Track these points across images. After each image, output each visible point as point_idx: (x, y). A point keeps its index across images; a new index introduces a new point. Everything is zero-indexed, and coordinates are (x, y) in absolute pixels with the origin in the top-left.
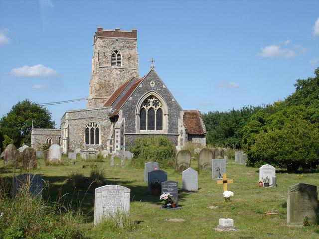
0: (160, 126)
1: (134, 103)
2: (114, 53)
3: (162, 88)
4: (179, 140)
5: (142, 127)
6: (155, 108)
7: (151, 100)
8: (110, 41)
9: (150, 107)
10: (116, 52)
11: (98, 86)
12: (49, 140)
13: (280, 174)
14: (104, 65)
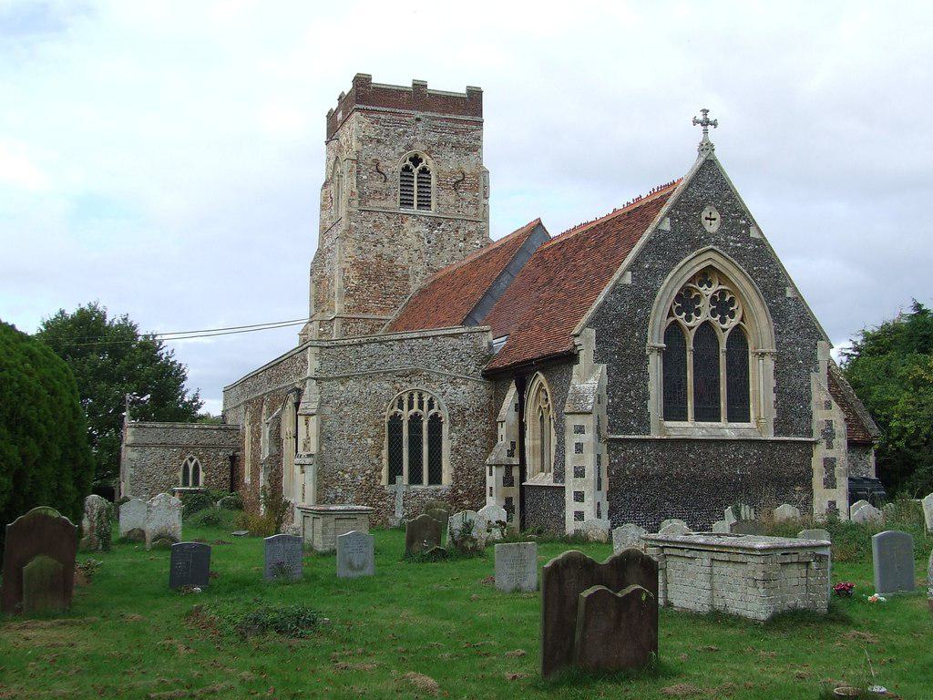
0: (739, 411)
1: (641, 296)
4: (817, 463)
5: (674, 410)
6: (718, 325)
7: (707, 292)
8: (400, 124)
9: (701, 319)
12: (191, 466)
14: (372, 204)
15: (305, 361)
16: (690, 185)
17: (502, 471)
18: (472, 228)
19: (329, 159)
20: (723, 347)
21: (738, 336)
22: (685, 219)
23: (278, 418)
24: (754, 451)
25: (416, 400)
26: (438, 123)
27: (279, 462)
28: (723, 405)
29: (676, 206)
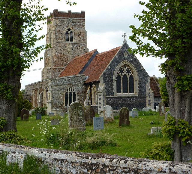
0: (132, 91)
1: (112, 70)
2: (67, 30)
3: (133, 58)
4: (147, 101)
6: (128, 75)
7: (125, 69)
10: (69, 30)
11: (55, 58)
13: (18, 130)
15: (48, 82)
16: (122, 49)
17: (87, 103)
18: (83, 46)
19: (47, 28)
20: (128, 79)
21: (132, 77)
22: (121, 55)
23: (42, 94)
24: (134, 99)
25: (70, 89)
26: (74, 20)
27: (43, 102)
28: (128, 90)
29: (119, 53)
